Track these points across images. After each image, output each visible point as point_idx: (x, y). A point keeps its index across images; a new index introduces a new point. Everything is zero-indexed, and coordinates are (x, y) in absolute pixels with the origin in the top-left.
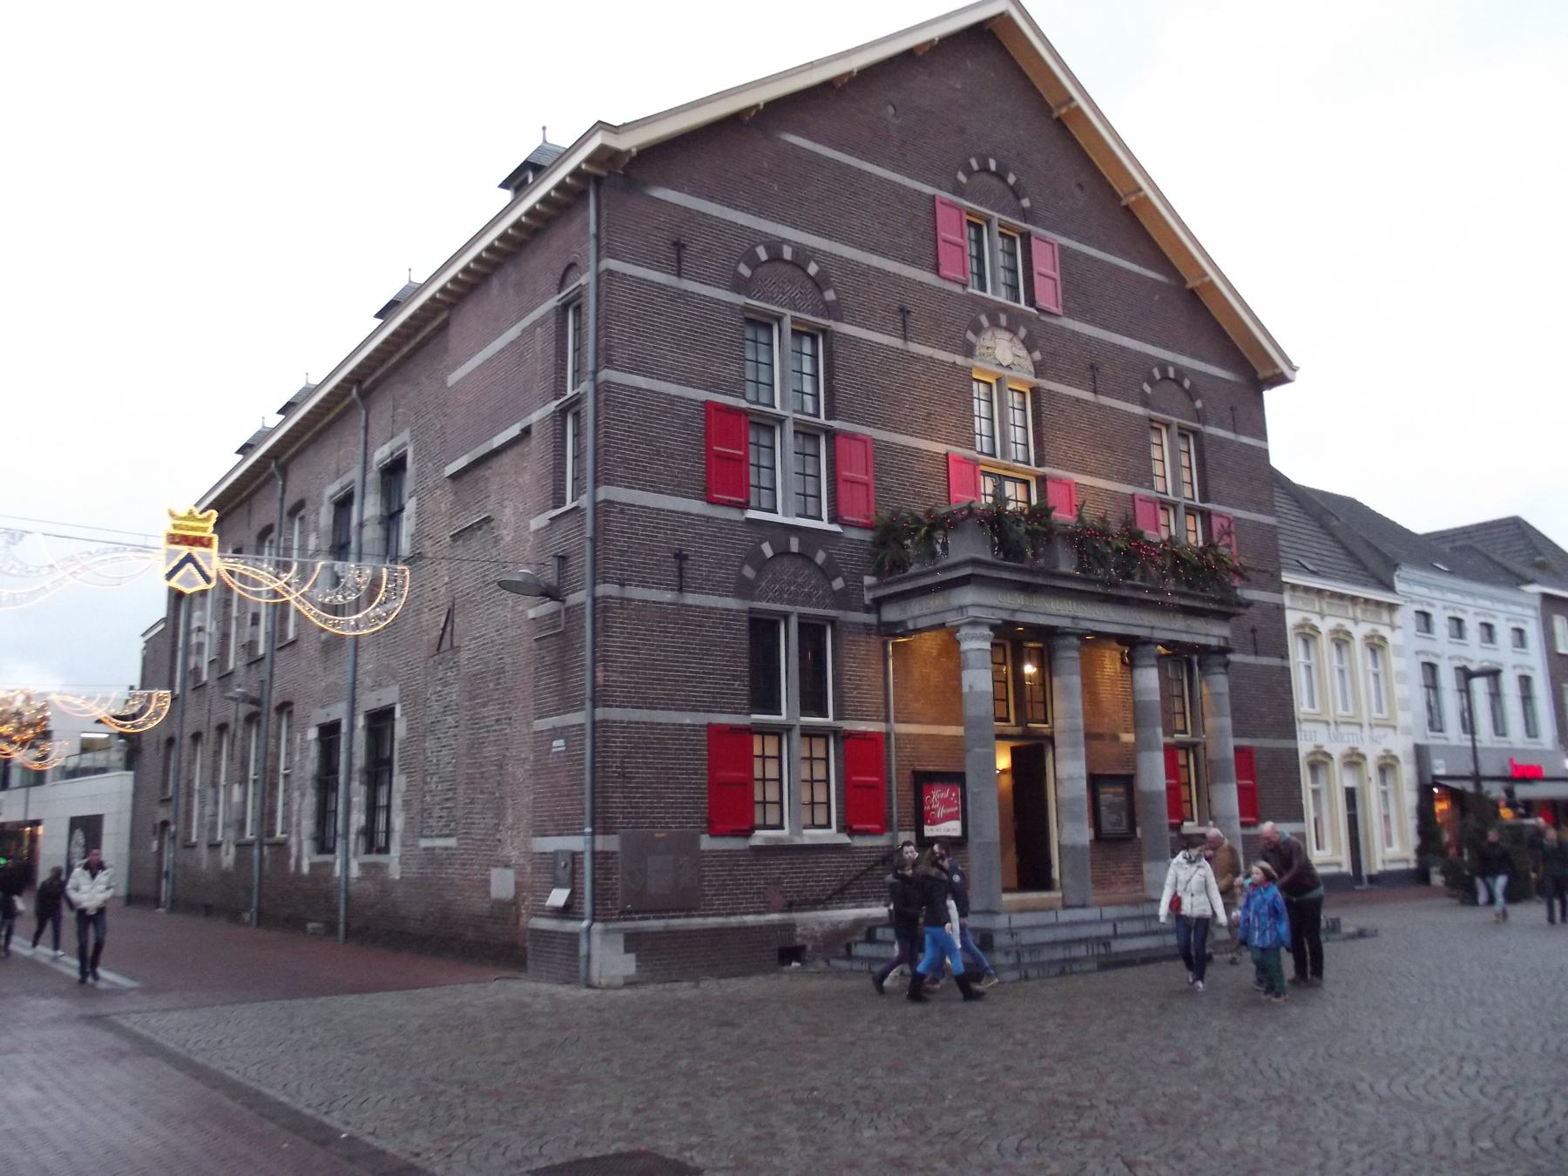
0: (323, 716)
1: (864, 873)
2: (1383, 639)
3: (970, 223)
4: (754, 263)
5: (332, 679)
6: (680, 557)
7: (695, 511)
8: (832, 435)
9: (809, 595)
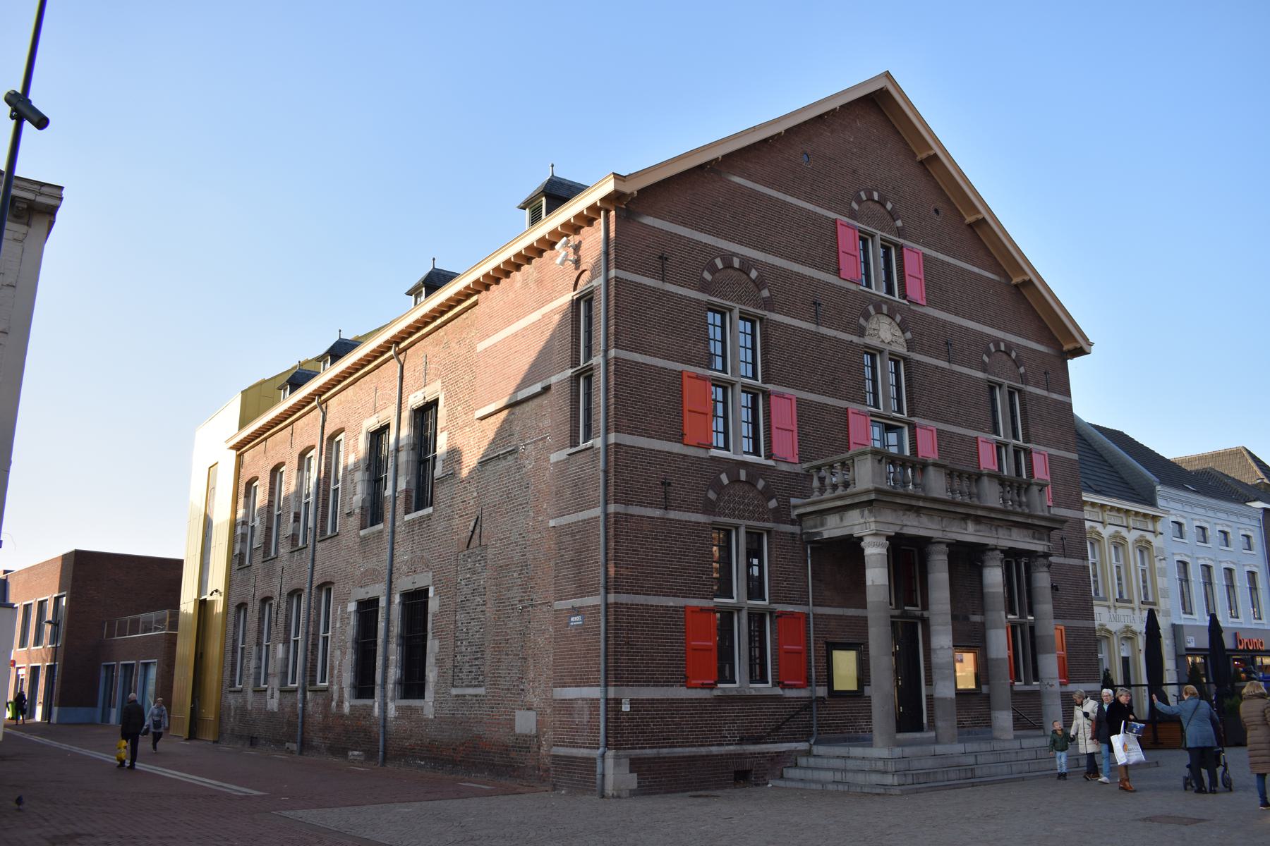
0: (363, 594)
1: (792, 716)
2: (1149, 542)
3: (861, 238)
4: (713, 269)
5: (369, 566)
6: (666, 484)
7: (675, 451)
8: (767, 395)
9: (753, 512)
